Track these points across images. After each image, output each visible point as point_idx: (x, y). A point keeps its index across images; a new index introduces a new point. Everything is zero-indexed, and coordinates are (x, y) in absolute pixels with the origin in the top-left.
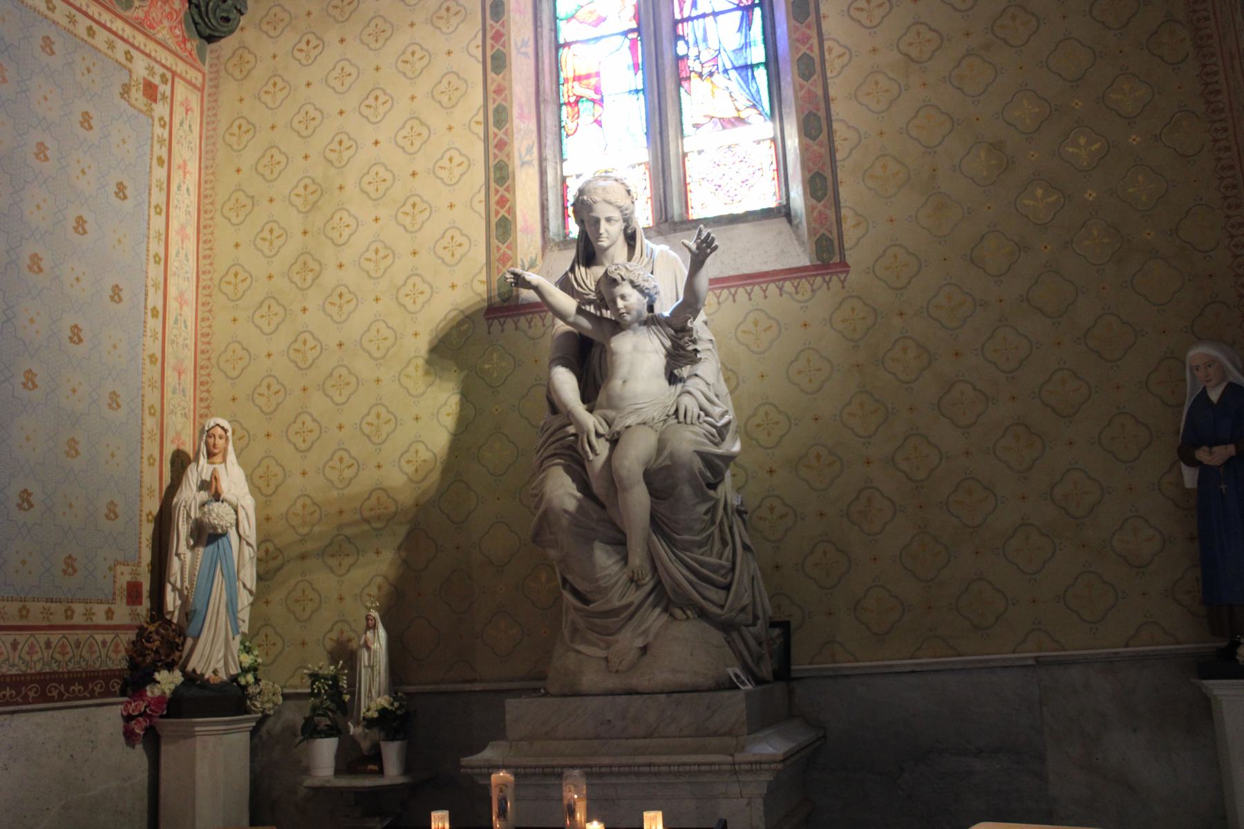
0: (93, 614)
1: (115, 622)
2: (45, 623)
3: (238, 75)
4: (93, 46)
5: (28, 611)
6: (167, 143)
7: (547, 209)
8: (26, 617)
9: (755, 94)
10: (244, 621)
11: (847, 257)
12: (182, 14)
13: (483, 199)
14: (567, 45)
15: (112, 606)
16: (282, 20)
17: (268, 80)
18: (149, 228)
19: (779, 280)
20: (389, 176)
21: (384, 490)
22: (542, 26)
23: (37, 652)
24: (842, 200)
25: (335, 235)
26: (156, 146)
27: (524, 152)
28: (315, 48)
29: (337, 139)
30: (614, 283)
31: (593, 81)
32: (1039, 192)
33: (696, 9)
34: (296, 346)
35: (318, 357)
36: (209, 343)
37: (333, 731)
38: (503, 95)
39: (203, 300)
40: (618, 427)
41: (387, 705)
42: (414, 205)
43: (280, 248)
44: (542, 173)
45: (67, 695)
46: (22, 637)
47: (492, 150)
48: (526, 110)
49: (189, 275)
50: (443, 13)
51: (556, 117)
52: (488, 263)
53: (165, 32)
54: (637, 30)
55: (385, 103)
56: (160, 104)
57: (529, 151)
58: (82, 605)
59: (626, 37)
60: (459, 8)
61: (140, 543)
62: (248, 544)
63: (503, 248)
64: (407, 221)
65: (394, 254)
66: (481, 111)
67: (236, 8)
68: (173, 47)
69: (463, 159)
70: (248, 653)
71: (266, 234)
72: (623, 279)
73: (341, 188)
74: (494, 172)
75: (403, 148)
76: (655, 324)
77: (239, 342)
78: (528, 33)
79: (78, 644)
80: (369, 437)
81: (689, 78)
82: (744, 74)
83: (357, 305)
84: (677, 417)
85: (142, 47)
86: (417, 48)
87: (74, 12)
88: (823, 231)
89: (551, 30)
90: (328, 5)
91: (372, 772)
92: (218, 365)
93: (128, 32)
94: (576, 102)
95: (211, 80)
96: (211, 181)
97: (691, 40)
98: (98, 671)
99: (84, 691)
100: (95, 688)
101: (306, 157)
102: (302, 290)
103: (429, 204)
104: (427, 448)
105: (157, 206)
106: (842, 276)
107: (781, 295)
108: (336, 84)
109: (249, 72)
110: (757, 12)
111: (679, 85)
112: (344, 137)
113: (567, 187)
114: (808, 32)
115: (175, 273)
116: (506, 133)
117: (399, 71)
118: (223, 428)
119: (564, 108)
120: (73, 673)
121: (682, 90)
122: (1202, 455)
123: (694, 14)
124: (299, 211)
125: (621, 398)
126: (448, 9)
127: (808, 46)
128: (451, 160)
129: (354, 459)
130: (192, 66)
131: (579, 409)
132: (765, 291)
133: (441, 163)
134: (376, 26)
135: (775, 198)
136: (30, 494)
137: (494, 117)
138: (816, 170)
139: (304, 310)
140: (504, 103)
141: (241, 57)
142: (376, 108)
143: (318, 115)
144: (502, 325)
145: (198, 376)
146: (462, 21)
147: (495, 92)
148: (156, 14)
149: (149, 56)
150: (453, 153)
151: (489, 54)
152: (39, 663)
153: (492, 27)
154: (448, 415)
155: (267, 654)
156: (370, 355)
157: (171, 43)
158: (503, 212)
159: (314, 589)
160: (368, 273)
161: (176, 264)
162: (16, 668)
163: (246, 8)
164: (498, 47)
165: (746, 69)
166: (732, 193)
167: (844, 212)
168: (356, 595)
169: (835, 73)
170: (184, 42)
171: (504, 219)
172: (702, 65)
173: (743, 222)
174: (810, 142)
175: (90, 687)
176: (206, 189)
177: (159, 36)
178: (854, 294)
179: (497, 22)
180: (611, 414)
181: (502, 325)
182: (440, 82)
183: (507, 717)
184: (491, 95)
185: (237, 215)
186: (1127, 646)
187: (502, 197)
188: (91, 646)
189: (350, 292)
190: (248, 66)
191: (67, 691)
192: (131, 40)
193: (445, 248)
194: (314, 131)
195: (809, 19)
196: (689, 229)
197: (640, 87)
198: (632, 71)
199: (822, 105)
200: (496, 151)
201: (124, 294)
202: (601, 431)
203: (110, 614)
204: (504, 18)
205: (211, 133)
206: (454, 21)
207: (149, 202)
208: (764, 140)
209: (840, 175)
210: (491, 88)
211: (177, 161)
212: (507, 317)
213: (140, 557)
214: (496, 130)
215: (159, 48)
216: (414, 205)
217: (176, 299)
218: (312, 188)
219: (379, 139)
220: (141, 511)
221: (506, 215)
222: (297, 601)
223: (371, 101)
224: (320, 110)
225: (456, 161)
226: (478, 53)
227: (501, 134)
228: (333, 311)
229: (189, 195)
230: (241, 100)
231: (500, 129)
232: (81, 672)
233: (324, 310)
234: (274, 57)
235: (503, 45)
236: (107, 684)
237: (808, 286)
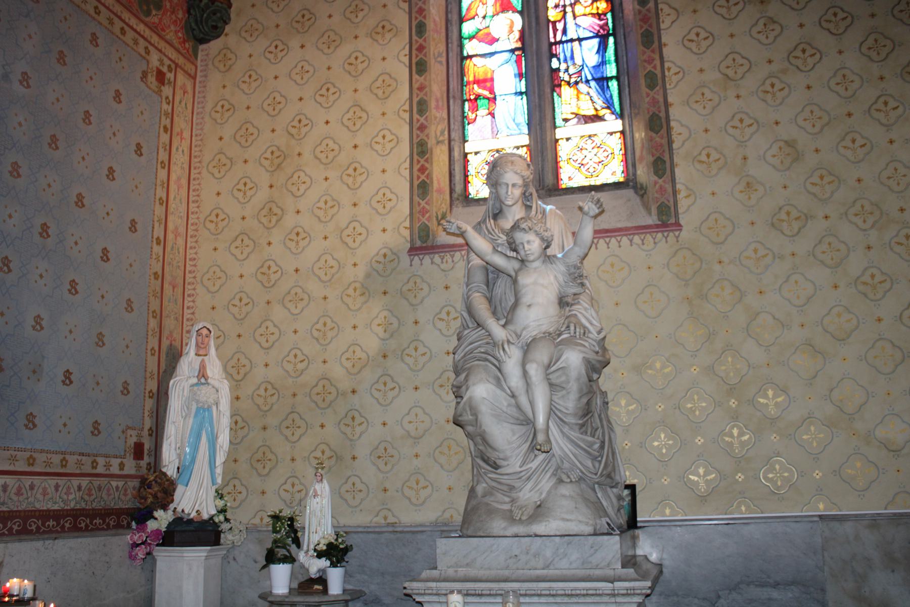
0: (111, 466)
1: (125, 472)
2: (78, 472)
3: (221, 67)
4: (124, 42)
5: (67, 461)
6: (170, 116)
7: (454, 176)
8: (65, 466)
9: (609, 99)
11: (680, 219)
12: (184, 22)
13: (408, 167)
14: (470, 57)
15: (124, 461)
16: (257, 30)
18: (156, 178)
19: (630, 234)
20: (336, 147)
22: (452, 43)
23: (72, 494)
24: (677, 178)
25: (294, 189)
26: (163, 118)
27: (438, 134)
28: (281, 51)
29: (298, 118)
31: (488, 84)
33: (566, 35)
34: (262, 270)
35: (279, 279)
36: (195, 266)
37: (289, 559)
38: (424, 91)
39: (192, 233)
41: (333, 541)
42: (355, 170)
43: (251, 197)
44: (450, 150)
45: (91, 526)
46: (61, 481)
47: (415, 132)
48: (440, 103)
49: (182, 214)
50: (380, 29)
51: (460, 110)
52: (411, 214)
53: (172, 34)
54: (522, 49)
55: (335, 93)
56: (167, 86)
57: (442, 133)
58: (103, 458)
59: (514, 53)
60: (391, 27)
61: (144, 413)
63: (423, 203)
64: (350, 181)
65: (339, 205)
66: (408, 102)
67: (222, 19)
68: (177, 45)
69: (393, 137)
70: (220, 498)
71: (241, 186)
73: (299, 154)
74: (417, 148)
75: (348, 127)
77: (218, 266)
78: (442, 48)
79: (100, 488)
80: (317, 340)
81: (560, 86)
82: (601, 84)
83: (310, 241)
85: (156, 45)
86: (359, 55)
87: (112, 16)
88: (663, 200)
89: (458, 46)
90: (292, 20)
91: (317, 592)
92: (202, 282)
93: (147, 33)
94: (476, 99)
95: (201, 71)
96: (200, 146)
97: (562, 57)
98: (113, 509)
99: (57, 526)
100: (13, 526)
101: (273, 131)
102: (268, 228)
103: (366, 169)
105: (162, 162)
106: (677, 233)
107: (631, 245)
108: (298, 78)
109: (231, 66)
110: (611, 40)
111: (553, 91)
112: (303, 117)
113: (468, 161)
114: (653, 55)
115: (173, 213)
116: (426, 119)
117: (346, 71)
118: (208, 329)
119: (466, 103)
120: (96, 510)
121: (555, 94)
123: (564, 39)
124: (267, 171)
126: (383, 27)
127: (652, 65)
128: (384, 137)
130: (188, 60)
132: (619, 242)
133: (376, 139)
134: (329, 37)
135: (623, 175)
136: (71, 373)
137: (417, 107)
138: (658, 155)
139: (269, 244)
140: (425, 98)
141: (225, 55)
142: (327, 97)
143: (283, 100)
144: (421, 260)
145: (186, 290)
146: (395, 36)
148: (166, 21)
149: (160, 51)
150: (386, 132)
151: (414, 61)
152: (73, 501)
153: (417, 42)
155: (235, 500)
156: (320, 278)
157: (176, 42)
158: (423, 177)
159: (272, 452)
160: (319, 218)
161: (173, 206)
162: (57, 505)
163: (230, 19)
164: (421, 56)
165: (602, 81)
166: (591, 170)
167: (678, 186)
168: (305, 457)
169: (672, 86)
170: (184, 42)
171: (424, 182)
172: (570, 76)
173: (625, 188)
174: (654, 135)
175: (107, 521)
176: (196, 151)
177: (168, 37)
179: (420, 38)
181: (421, 260)
182: (377, 80)
183: (438, 551)
184: (415, 91)
185: (219, 172)
186: (886, 509)
187: (423, 166)
188: (108, 490)
189: (304, 232)
190: (230, 62)
191: (91, 523)
192: (149, 39)
193: (378, 202)
194: (280, 112)
195: (654, 46)
196: (560, 195)
197: (524, 90)
198: (518, 79)
199: (663, 108)
200: (418, 132)
201: (138, 226)
203: (122, 466)
204: (426, 35)
205: (200, 110)
206: (388, 36)
207: (157, 159)
208: (615, 132)
209: (675, 160)
210: (415, 86)
211: (176, 130)
212: (425, 254)
213: (143, 424)
214: (418, 117)
215: (167, 46)
216: (355, 170)
217: (173, 233)
218: (277, 154)
219: (329, 120)
220: (145, 389)
221: (426, 180)
222: (258, 461)
223: (324, 91)
224: (284, 97)
225: (387, 139)
226: (406, 60)
227: (422, 120)
228: (292, 245)
229: (184, 155)
230: (224, 87)
231: (422, 117)
232: (101, 510)
233: (284, 243)
234: (250, 56)
235: (425, 55)
236: (25, 524)
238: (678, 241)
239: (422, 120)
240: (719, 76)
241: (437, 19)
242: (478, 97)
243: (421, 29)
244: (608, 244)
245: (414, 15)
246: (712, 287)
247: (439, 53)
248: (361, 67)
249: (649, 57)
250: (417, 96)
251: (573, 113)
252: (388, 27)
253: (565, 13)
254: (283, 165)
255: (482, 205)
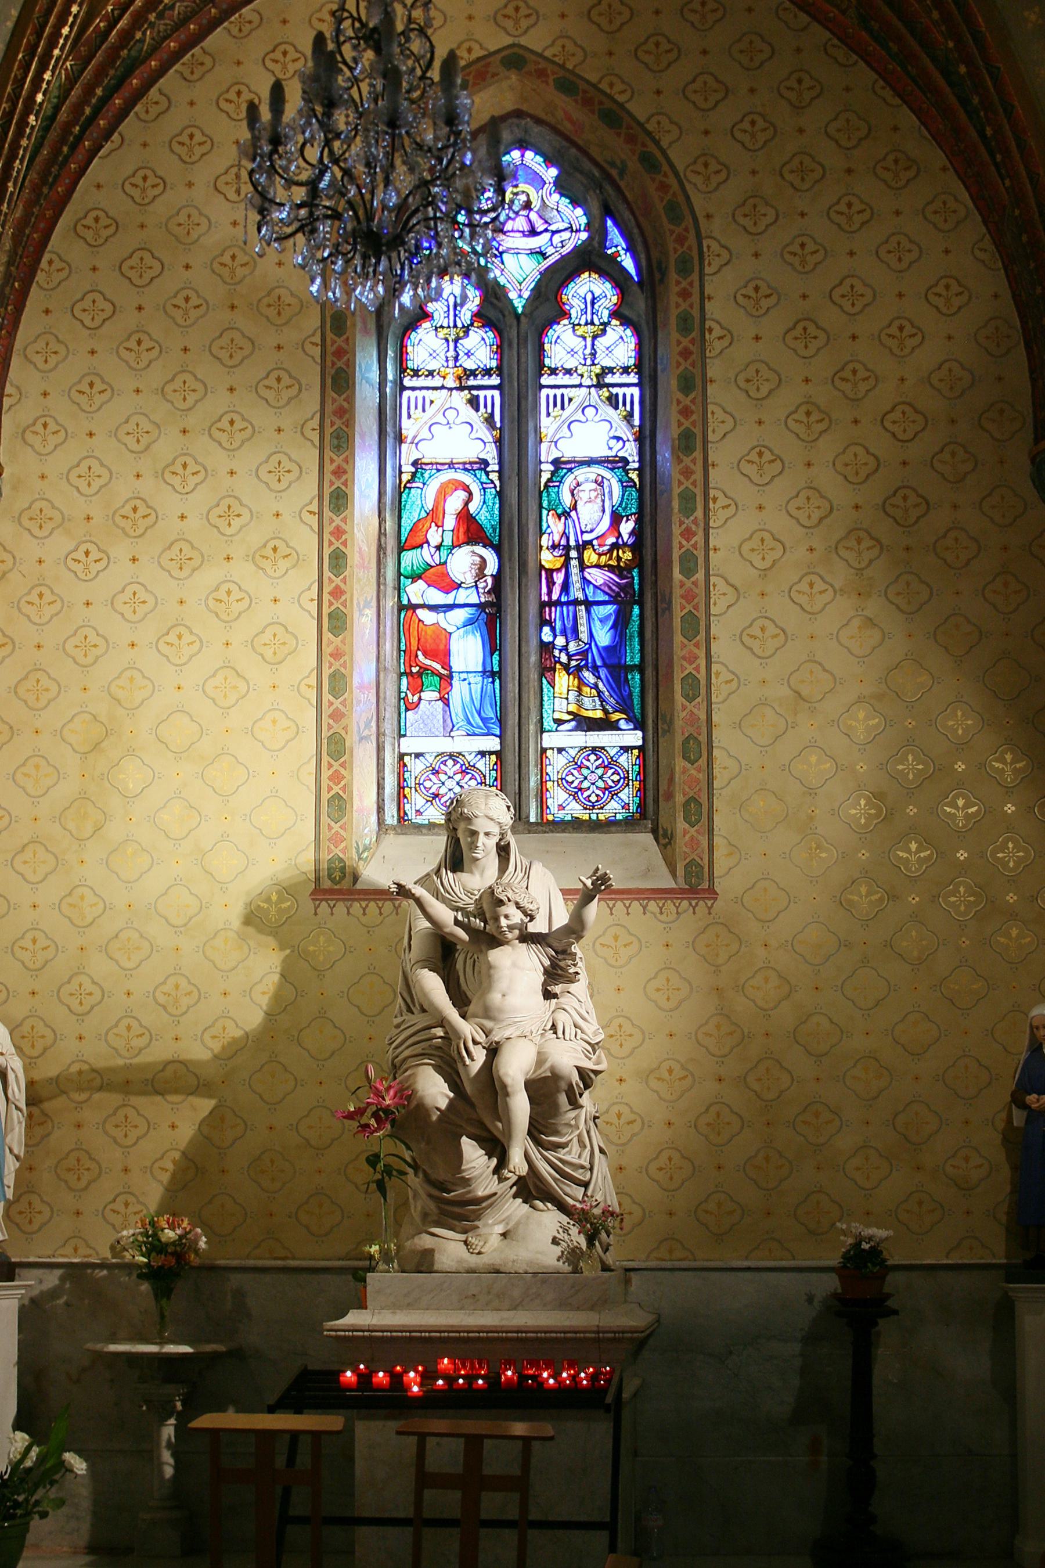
7: (383, 788)
10: (9, 1187)
17: (32, 588)
19: (644, 899)
21: (180, 1062)
27: (362, 727)
30: (500, 903)
32: (913, 846)
33: (567, 594)
40: (496, 1037)
44: (380, 749)
51: (396, 687)
57: (367, 725)
62: (17, 1108)
63: (336, 827)
72: (509, 900)
76: (533, 943)
80: (164, 1008)
84: (555, 1033)
94: (420, 674)
97: (558, 625)
104: (237, 1026)
106: (710, 903)
107: (644, 913)
108: (127, 610)
114: (695, 650)
122: (1031, 1099)
123: (564, 599)
125: (501, 1010)
127: (694, 666)
129: (145, 1027)
131: (452, 1014)
132: (627, 908)
140: (342, 670)
146: (294, 567)
147: (331, 655)
151: (326, 611)
153: (330, 580)
154: (264, 993)
167: (717, 840)
172: (570, 657)
178: (721, 920)
180: (489, 1024)
184: (327, 658)
195: (698, 638)
199: (704, 730)
200: (331, 722)
202: (478, 1039)
206: (283, 564)
210: (327, 650)
212: (338, 900)
214: (331, 698)
223: (172, 638)
227: (337, 703)
237: (674, 909)
238: (710, 913)
239: (337, 703)
240: (789, 692)
241: (365, 548)
242: (424, 669)
243: (338, 561)
244: (611, 909)
245: (327, 536)
246: (753, 977)
247: (366, 601)
248: (237, 608)
249: (691, 652)
250: (330, 667)
251: (569, 713)
252: (283, 549)
253: (568, 559)
254: (103, 745)
255: (425, 835)
